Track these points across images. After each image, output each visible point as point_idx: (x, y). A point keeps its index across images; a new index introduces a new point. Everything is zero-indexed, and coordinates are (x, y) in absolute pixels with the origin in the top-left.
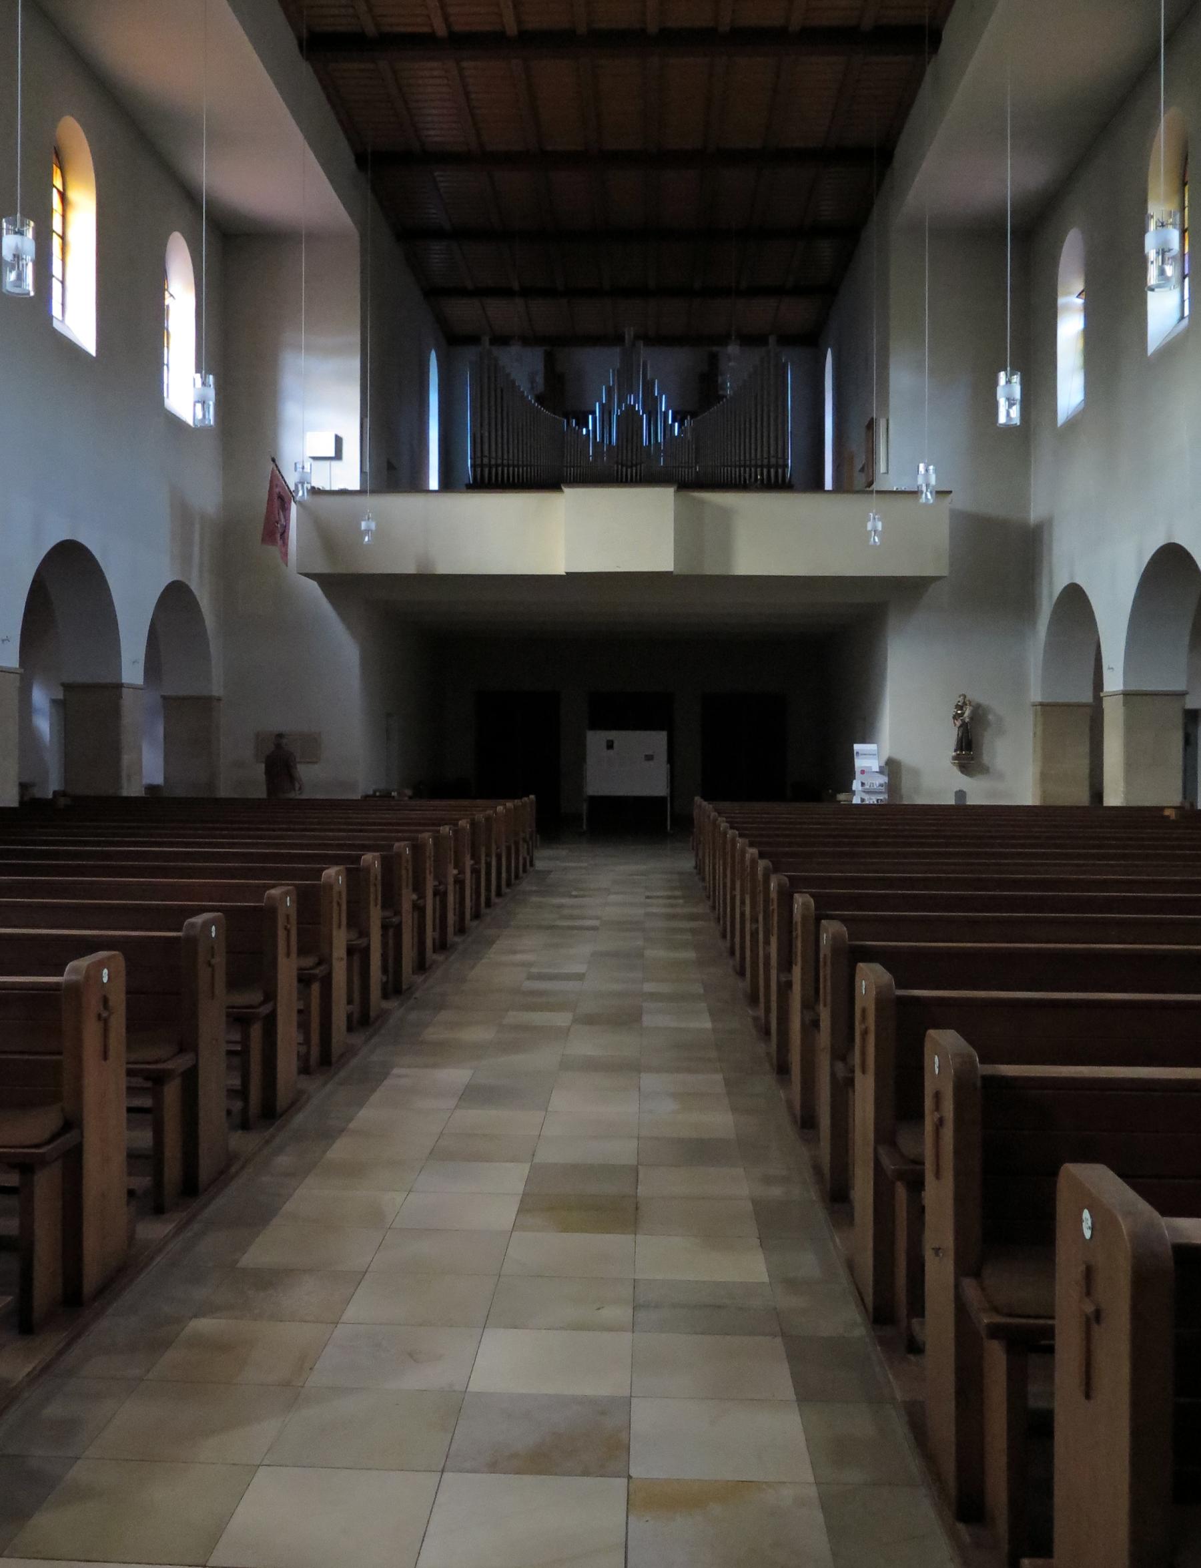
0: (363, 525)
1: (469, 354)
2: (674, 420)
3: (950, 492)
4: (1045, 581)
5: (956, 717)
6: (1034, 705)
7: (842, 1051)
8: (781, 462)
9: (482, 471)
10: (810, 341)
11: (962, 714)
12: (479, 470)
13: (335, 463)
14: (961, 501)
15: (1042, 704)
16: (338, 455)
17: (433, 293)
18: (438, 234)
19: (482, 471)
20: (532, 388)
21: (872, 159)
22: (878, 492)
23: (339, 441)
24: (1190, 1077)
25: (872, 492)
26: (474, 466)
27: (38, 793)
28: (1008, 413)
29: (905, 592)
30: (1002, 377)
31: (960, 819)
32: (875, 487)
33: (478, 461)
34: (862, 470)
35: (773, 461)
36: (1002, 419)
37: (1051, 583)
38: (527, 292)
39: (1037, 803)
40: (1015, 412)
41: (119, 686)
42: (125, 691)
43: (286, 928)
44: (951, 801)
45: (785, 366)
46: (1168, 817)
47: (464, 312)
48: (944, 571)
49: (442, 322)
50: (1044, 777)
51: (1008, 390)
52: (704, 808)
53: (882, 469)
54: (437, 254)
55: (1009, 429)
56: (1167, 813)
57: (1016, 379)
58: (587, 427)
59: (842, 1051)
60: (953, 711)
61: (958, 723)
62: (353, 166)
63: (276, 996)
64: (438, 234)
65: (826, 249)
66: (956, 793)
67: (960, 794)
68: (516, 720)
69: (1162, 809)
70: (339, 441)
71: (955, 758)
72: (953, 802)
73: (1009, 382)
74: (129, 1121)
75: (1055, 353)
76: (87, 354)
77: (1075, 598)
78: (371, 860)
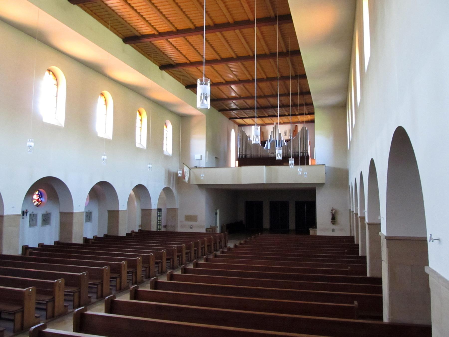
2: (285, 142)
5: (331, 212)
13: (201, 161)
16: (201, 159)
70: (201, 156)
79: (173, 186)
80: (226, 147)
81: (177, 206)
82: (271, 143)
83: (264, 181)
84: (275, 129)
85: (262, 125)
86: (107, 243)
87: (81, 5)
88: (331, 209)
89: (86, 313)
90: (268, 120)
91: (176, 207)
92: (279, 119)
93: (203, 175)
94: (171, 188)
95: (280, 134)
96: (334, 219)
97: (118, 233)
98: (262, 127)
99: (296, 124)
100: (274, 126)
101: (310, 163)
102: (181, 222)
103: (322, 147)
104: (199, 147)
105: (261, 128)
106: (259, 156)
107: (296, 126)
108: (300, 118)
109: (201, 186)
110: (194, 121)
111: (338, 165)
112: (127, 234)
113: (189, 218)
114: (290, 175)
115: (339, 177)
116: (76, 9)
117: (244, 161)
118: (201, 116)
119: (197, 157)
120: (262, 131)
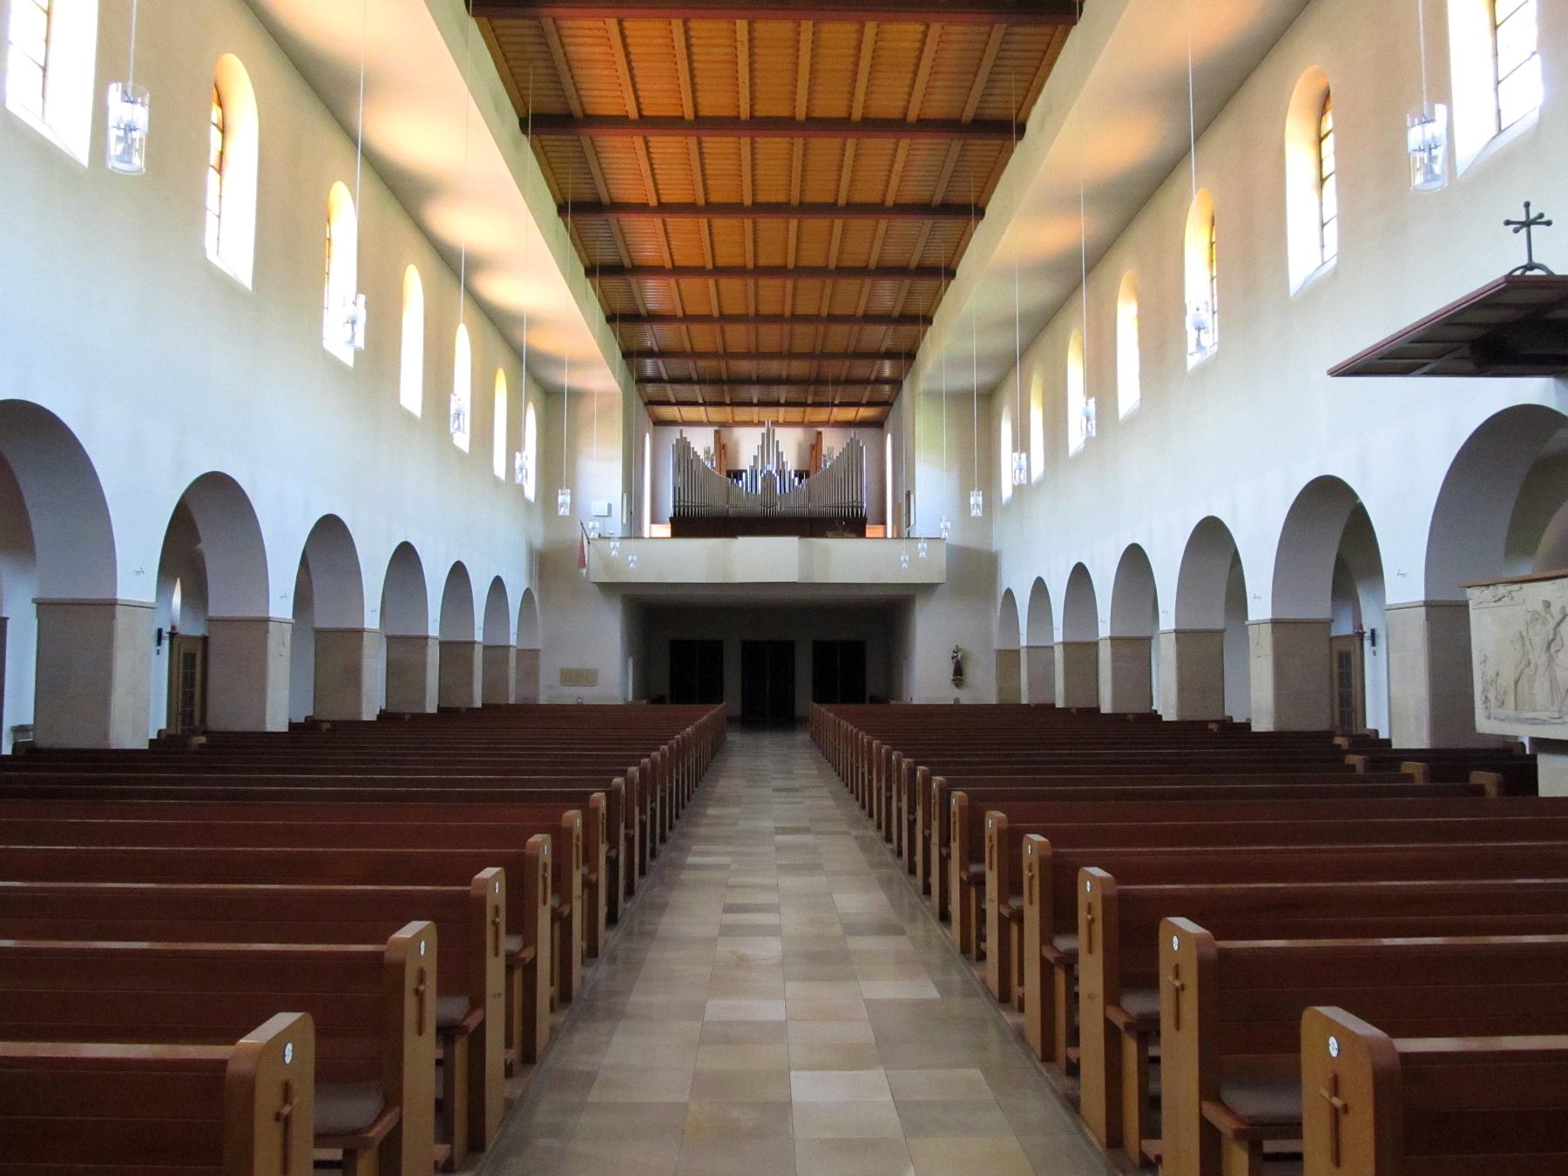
7: (945, 842)
10: (878, 424)
16: (610, 514)
17: (651, 403)
21: (907, 356)
23: (610, 506)
27: (225, 715)
29: (928, 588)
41: (109, 606)
42: (119, 610)
43: (417, 992)
46: (1339, 746)
49: (652, 415)
50: (1000, 691)
51: (976, 498)
56: (1211, 726)
59: (945, 842)
63: (401, 1099)
65: (887, 388)
68: (767, 669)
69: (1205, 723)
70: (610, 506)
74: (317, 1092)
77: (1009, 592)
78: (599, 797)
82: (764, 479)
84: (767, 440)
85: (722, 426)
86: (204, 752)
87: (485, 20)
89: (426, 923)
90: (743, 414)
92: (782, 413)
95: (779, 455)
96: (959, 672)
97: (106, 735)
98: (724, 431)
100: (764, 430)
101: (646, 535)
102: (550, 687)
103: (933, 493)
104: (600, 480)
106: (779, 508)
108: (822, 414)
110: (594, 406)
111: (973, 541)
112: (292, 726)
113: (570, 677)
114: (845, 562)
115: (975, 571)
116: (472, 25)
117: (685, 525)
118: (612, 394)
120: (724, 441)
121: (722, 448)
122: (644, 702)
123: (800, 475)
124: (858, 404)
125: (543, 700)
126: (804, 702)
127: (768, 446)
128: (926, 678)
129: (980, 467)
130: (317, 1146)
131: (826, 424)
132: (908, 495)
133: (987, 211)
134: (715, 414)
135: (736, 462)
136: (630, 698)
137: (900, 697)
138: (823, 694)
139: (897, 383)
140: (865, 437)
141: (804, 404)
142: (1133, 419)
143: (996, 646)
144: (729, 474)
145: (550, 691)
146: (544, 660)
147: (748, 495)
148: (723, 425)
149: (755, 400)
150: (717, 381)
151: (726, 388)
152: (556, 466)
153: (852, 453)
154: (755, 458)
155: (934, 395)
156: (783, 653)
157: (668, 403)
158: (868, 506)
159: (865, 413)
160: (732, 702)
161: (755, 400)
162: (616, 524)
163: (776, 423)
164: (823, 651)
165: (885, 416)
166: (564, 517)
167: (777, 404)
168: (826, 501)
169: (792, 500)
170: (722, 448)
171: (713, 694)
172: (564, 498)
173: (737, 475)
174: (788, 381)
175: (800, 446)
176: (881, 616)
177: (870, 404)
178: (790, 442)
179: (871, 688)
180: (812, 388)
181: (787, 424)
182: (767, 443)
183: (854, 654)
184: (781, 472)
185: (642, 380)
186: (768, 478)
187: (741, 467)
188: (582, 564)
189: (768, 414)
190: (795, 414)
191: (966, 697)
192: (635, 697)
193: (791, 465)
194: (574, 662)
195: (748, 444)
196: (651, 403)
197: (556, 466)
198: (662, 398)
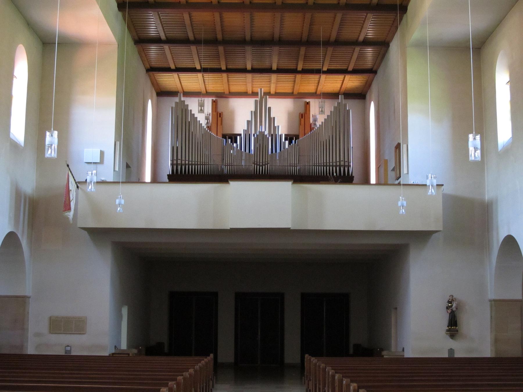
0: (117, 201)
1: (172, 102)
2: (286, 139)
3: (443, 185)
4: (495, 233)
5: (447, 308)
6: (490, 301)
8: (346, 164)
9: (177, 167)
10: (360, 95)
11: (451, 306)
12: (175, 167)
13: (100, 167)
14: (447, 189)
15: (495, 301)
16: (102, 161)
17: (151, 70)
18: (157, 41)
19: (177, 167)
20: (207, 123)
22: (403, 185)
24: (190, 223)
25: (399, 184)
26: (172, 165)
28: (474, 154)
29: (422, 237)
30: (471, 136)
31: (451, 366)
32: (402, 181)
33: (175, 162)
34: (393, 170)
35: (342, 163)
36: (472, 158)
37: (498, 233)
38: (205, 70)
39: (493, 356)
40: (479, 152)
44: (446, 355)
45: (348, 112)
47: (170, 80)
48: (441, 229)
49: (155, 84)
50: (496, 341)
51: (474, 141)
52: (312, 361)
53: (405, 171)
54: (153, 50)
55: (475, 163)
57: (478, 137)
58: (236, 142)
60: (446, 304)
61: (449, 311)
62: (116, 8)
64: (157, 41)
65: (369, 51)
66: (449, 350)
67: (451, 351)
70: (102, 153)
71: (447, 331)
72: (447, 356)
73: (475, 139)
75: (497, 123)
76: (21, 146)
79: (23, 232)
80: (140, 141)
81: (27, 290)
83: (283, 220)
88: (448, 298)
90: (239, 82)
91: (27, 294)
93: (123, 202)
94: (20, 236)
95: (272, 120)
96: (453, 325)
98: (221, 102)
99: (308, 100)
102: (38, 335)
103: (425, 139)
104: (94, 125)
105: (214, 103)
107: (308, 103)
108: (309, 83)
109: (99, 234)
113: (59, 325)
114: (343, 209)
119: (91, 154)
120: (220, 110)
121: (218, 116)
122: (135, 351)
123: (290, 138)
124: (344, 72)
125: (31, 350)
126: (292, 351)
127: (259, 110)
128: (419, 330)
129: (471, 112)
130: (305, 297)
131: (314, 95)
132: (398, 147)
133: (409, 8)
134: (214, 82)
135: (232, 126)
136: (124, 346)
137: (388, 348)
138: (311, 346)
139: (382, 45)
140: (351, 106)
141: (294, 71)
142: (508, 149)
143: (492, 295)
144: (224, 136)
145: (39, 340)
146: (33, 309)
147: (241, 155)
148: (221, 95)
149: (249, 67)
150: (212, 42)
151: (221, 49)
152: (49, 108)
153: (339, 123)
154: (249, 122)
155: (420, 45)
156: (274, 303)
157: (168, 70)
158: (354, 168)
159: (352, 82)
160: (226, 350)
161: (249, 67)
162: (109, 170)
163: (268, 94)
164: (310, 303)
165: (368, 85)
166: (51, 159)
167: (269, 71)
168: (313, 161)
169: (284, 156)
170: (218, 116)
171: (207, 346)
172: (52, 138)
173: (233, 138)
174: (280, 42)
175: (290, 115)
176: (368, 268)
177: (355, 72)
178: (281, 111)
179: (357, 336)
180: (303, 50)
181: (278, 95)
182: (261, 112)
183: (340, 304)
184: (274, 136)
185: (142, 41)
186: (261, 138)
187: (237, 132)
188: (68, 208)
189: (261, 83)
190: (285, 82)
191: (461, 349)
192: (129, 346)
193: (282, 130)
194: (64, 309)
195: (241, 113)
196: (151, 70)
197: (49, 108)
198: (165, 65)
